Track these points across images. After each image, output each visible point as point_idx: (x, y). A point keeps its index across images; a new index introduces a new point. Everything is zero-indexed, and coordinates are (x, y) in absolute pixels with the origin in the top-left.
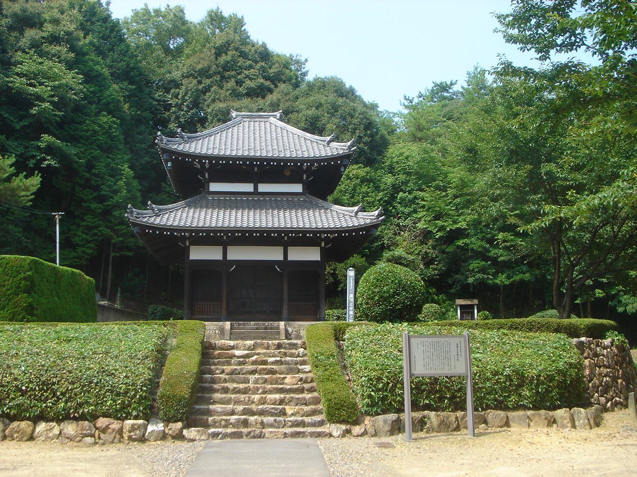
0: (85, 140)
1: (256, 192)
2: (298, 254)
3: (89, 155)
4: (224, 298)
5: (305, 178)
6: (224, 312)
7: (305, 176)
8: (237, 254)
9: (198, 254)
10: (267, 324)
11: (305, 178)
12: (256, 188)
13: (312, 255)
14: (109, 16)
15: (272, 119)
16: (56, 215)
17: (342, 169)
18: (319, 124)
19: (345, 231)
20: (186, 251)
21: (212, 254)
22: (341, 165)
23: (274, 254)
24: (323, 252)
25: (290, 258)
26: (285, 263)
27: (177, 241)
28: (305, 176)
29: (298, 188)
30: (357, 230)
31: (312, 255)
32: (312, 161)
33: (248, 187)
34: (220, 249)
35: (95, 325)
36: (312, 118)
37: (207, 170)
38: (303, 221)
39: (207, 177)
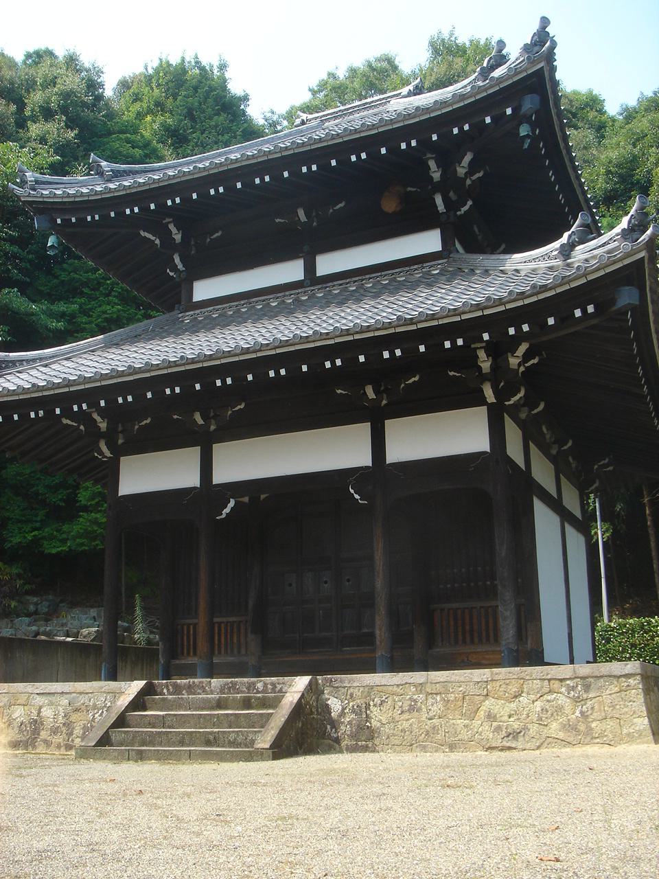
0: (92, 290)
2: (420, 440)
3: (99, 316)
4: (202, 605)
5: (441, 207)
8: (247, 462)
10: (260, 686)
11: (441, 207)
12: (310, 268)
14: (224, 87)
18: (639, 174)
26: (380, 472)
29: (429, 242)
33: (292, 271)
34: (192, 455)
35: (91, 683)
36: (619, 166)
39: (180, 267)
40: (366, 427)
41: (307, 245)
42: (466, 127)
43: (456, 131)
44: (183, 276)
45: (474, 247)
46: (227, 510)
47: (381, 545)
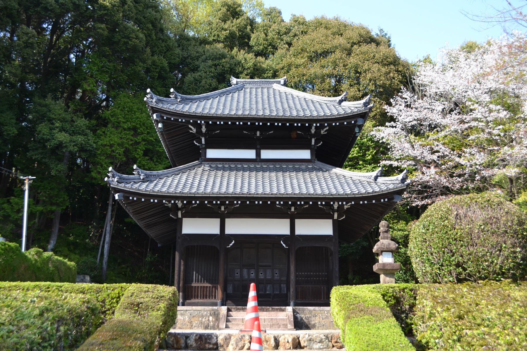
1: (258, 159)
2: (307, 228)
5: (313, 143)
6: (219, 293)
7: (313, 141)
8: (237, 227)
9: (191, 227)
11: (313, 143)
12: (258, 154)
13: (323, 228)
15: (276, 86)
16: (25, 180)
17: (357, 130)
19: (363, 198)
20: (179, 223)
21: (208, 227)
22: (355, 125)
23: (278, 227)
24: (336, 225)
25: (298, 232)
26: (292, 238)
27: (168, 211)
28: (313, 141)
29: (305, 154)
30: (378, 197)
31: (323, 228)
32: (322, 121)
33: (250, 154)
34: (217, 222)
37: (204, 135)
38: (313, 187)
39: (203, 142)
40: (219, 220)
41: (258, 145)
42: (338, 124)
43: (334, 124)
44: (204, 146)
45: (320, 160)
46: (231, 245)
47: (293, 265)
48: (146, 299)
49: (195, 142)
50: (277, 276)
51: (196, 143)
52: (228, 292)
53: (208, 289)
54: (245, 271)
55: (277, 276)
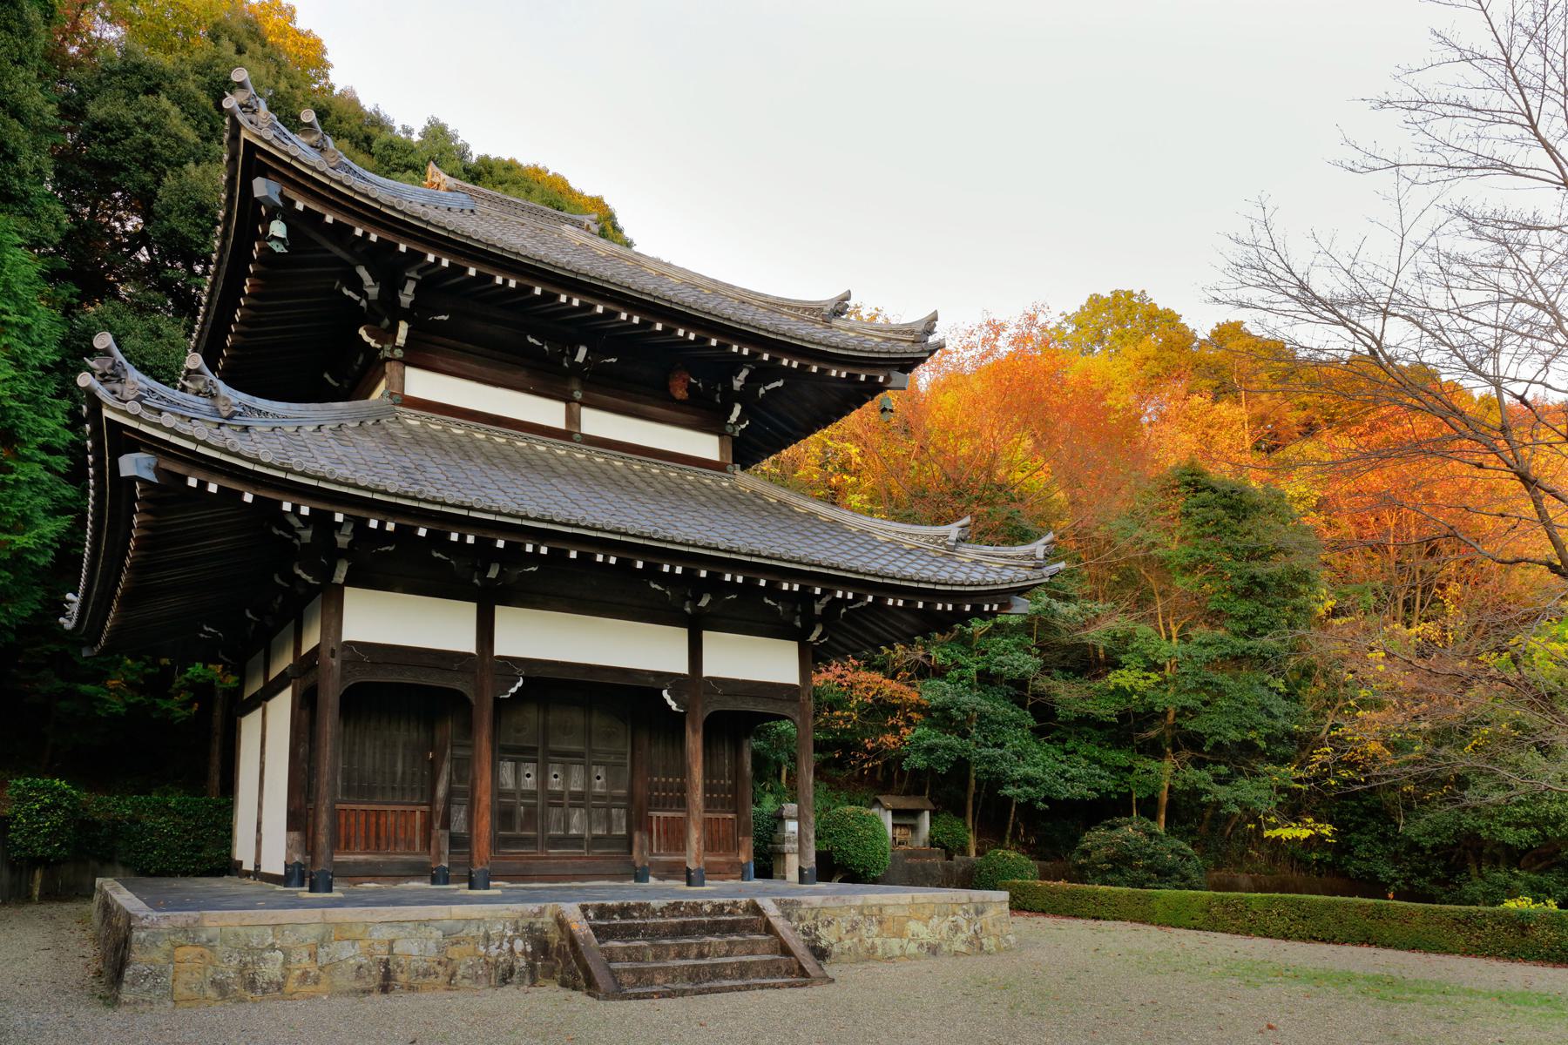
12: (573, 419)
25: (710, 669)
26: (692, 682)
48: (413, 949)
49: (362, 332)
50: (599, 787)
51: (366, 338)
52: (455, 828)
53: (373, 819)
54: (507, 770)
55: (599, 787)
